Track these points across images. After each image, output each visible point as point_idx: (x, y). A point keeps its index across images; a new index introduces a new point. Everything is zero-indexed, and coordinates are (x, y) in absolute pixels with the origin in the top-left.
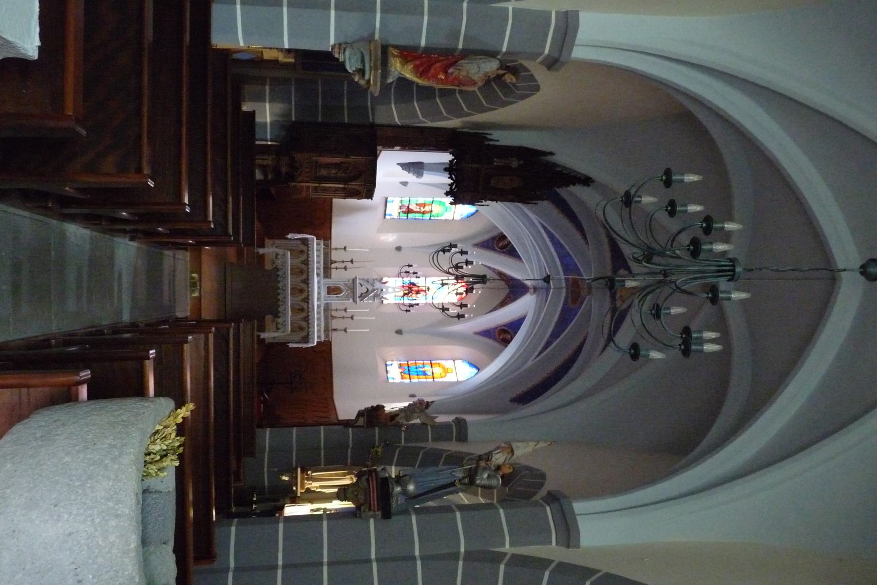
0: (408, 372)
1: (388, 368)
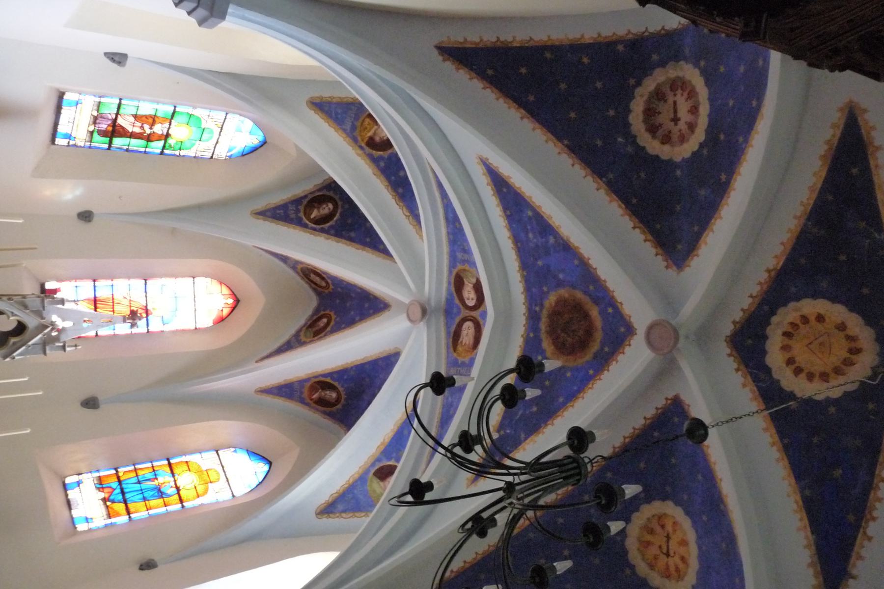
0: (120, 497)
1: (71, 494)
